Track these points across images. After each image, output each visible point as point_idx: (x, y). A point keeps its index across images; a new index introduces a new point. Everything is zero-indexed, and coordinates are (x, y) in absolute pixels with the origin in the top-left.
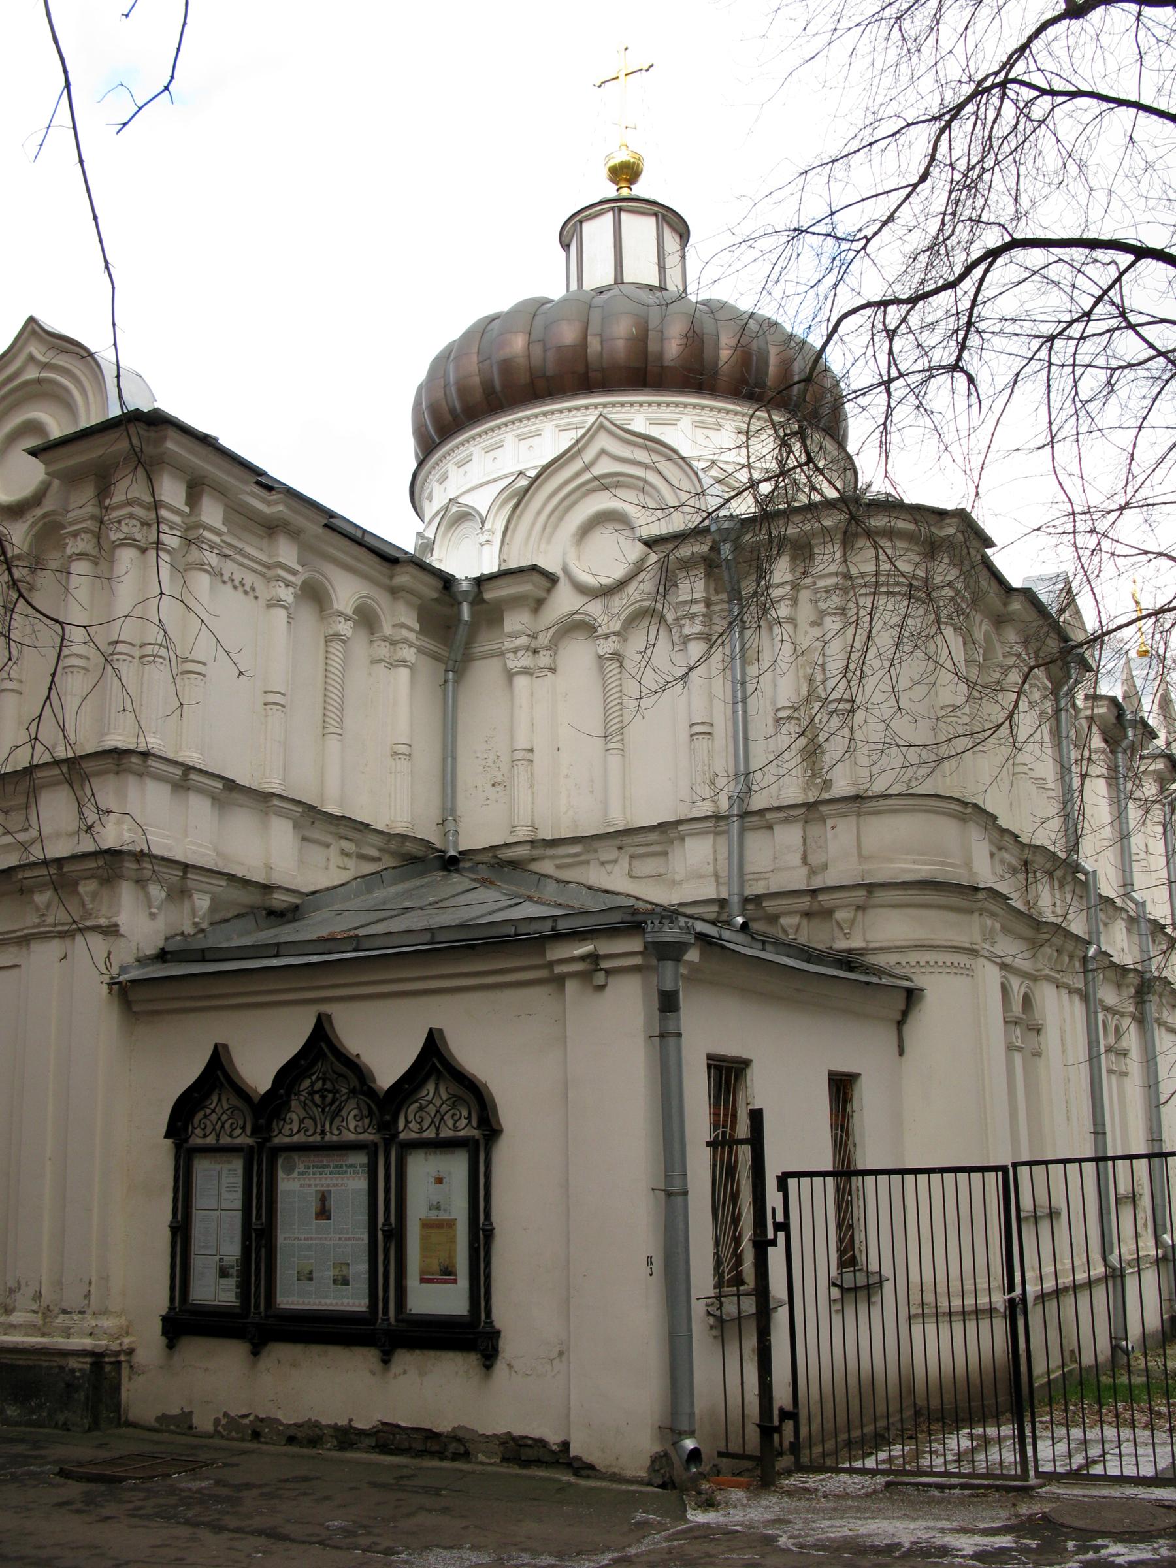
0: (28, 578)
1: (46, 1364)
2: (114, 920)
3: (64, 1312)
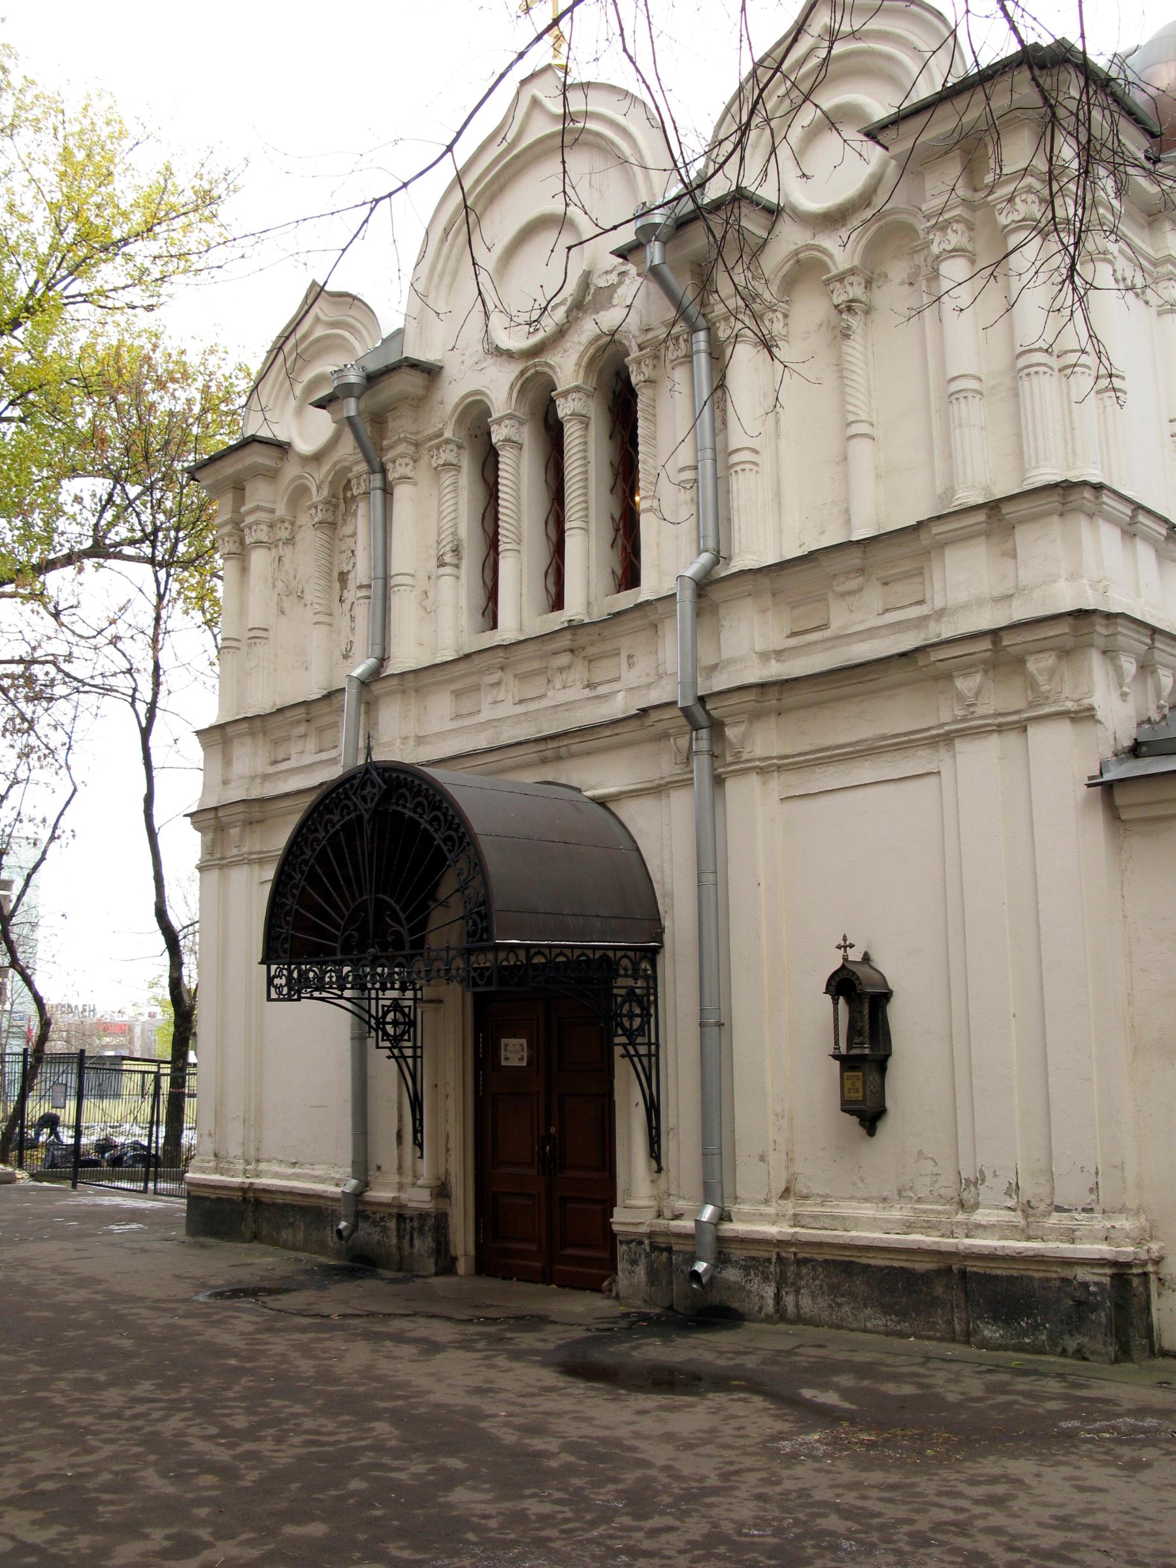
0: (863, 299)
1: (1041, 1275)
2: (1086, 702)
3: (1059, 1209)
